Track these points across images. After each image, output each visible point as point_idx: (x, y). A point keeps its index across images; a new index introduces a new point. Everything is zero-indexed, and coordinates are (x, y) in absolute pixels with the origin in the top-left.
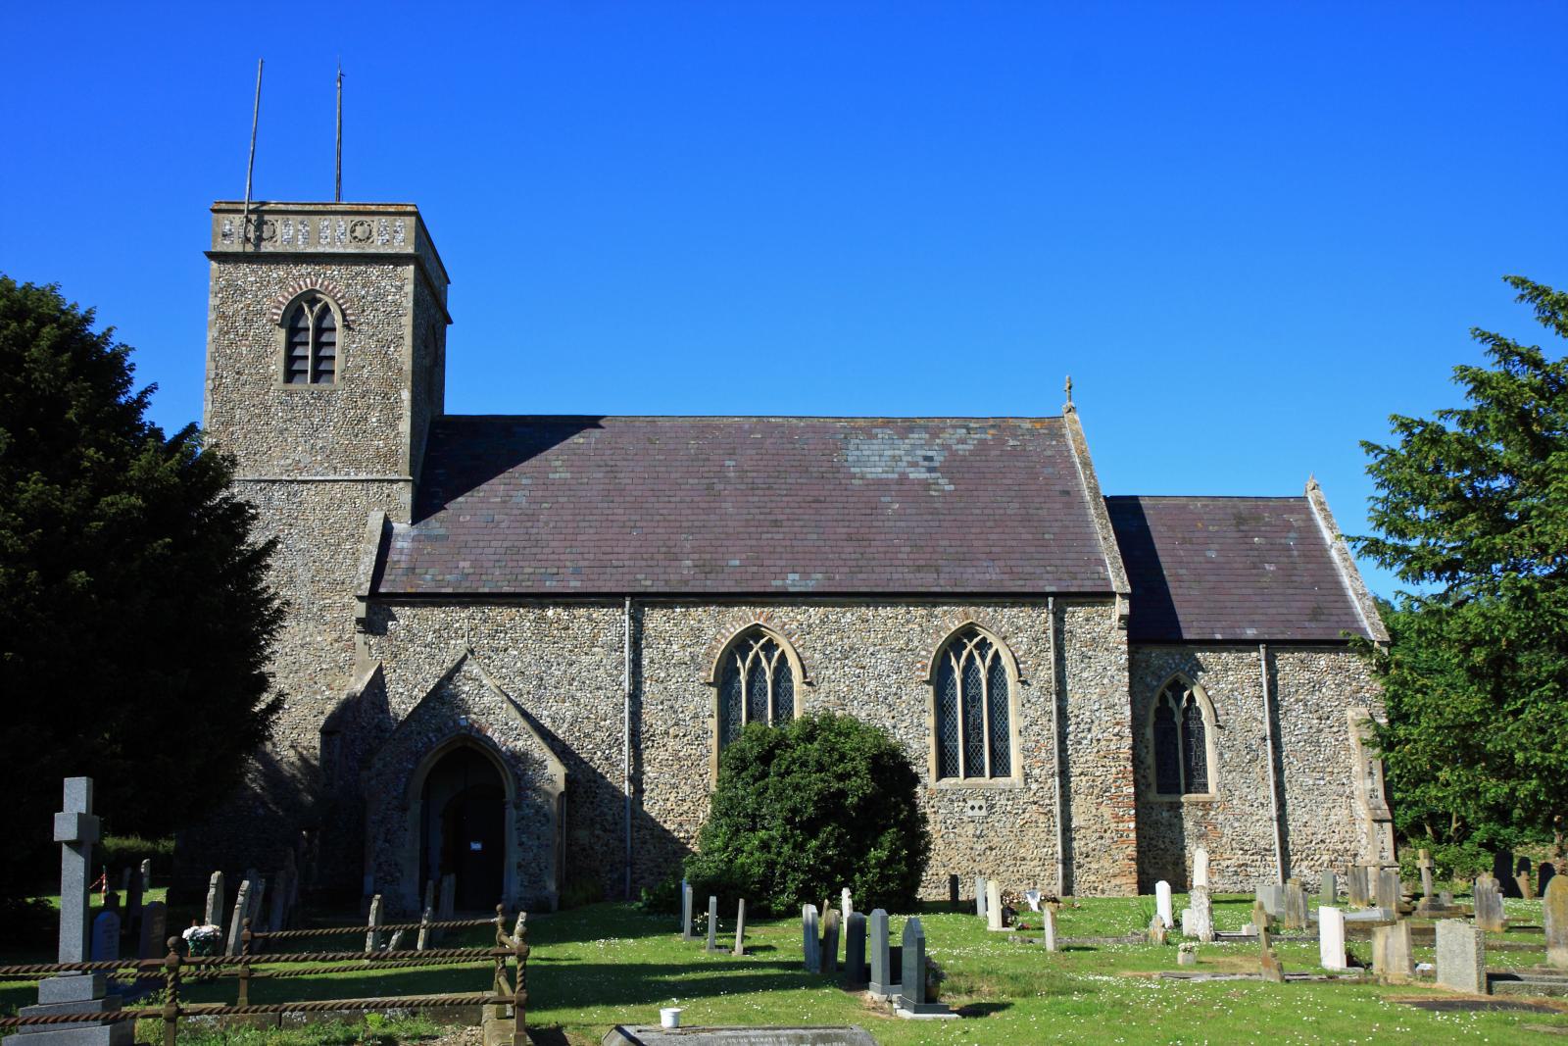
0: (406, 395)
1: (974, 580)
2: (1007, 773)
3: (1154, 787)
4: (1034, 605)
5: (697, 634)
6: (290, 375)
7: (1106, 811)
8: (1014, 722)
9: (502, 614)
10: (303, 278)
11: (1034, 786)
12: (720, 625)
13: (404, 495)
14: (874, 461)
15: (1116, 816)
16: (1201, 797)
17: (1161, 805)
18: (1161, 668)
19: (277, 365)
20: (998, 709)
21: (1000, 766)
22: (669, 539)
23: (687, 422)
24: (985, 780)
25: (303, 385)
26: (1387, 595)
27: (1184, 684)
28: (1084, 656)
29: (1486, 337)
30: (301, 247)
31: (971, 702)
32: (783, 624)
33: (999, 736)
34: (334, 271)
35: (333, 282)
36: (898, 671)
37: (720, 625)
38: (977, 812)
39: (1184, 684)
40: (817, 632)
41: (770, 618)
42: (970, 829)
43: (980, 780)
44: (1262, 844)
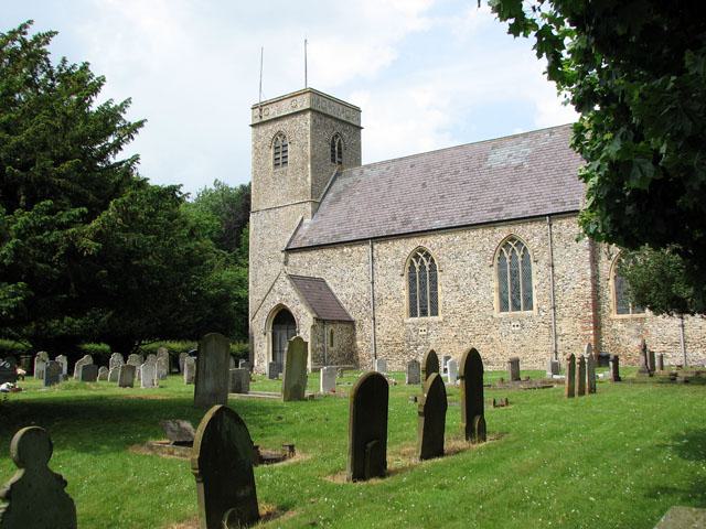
0: (309, 166)
1: (517, 212)
2: (531, 308)
3: (614, 311)
4: (541, 221)
7: (578, 325)
8: (535, 282)
9: (328, 252)
10: (277, 127)
11: (543, 314)
12: (406, 248)
13: (309, 207)
14: (497, 158)
15: (582, 327)
17: (617, 320)
19: (271, 163)
20: (528, 277)
21: (529, 306)
22: (51, 212)
29: (140, 124)
30: (277, 115)
31: (514, 274)
33: (529, 290)
34: (286, 122)
35: (284, 126)
36: (479, 262)
37: (406, 248)
38: (516, 328)
42: (513, 336)
43: (518, 312)
44: (675, 339)
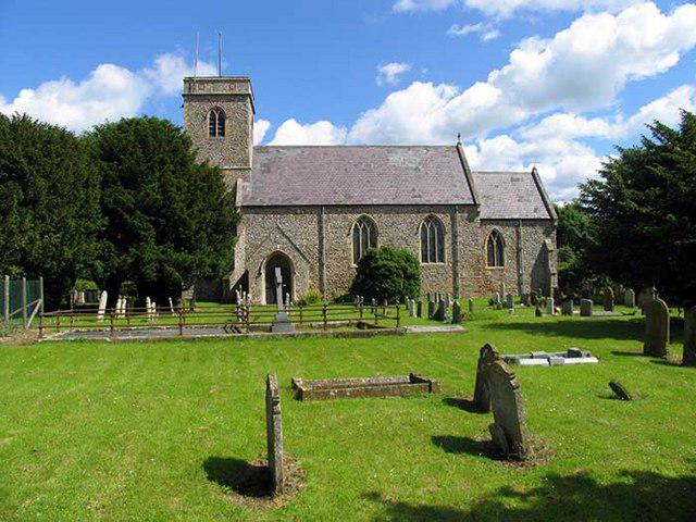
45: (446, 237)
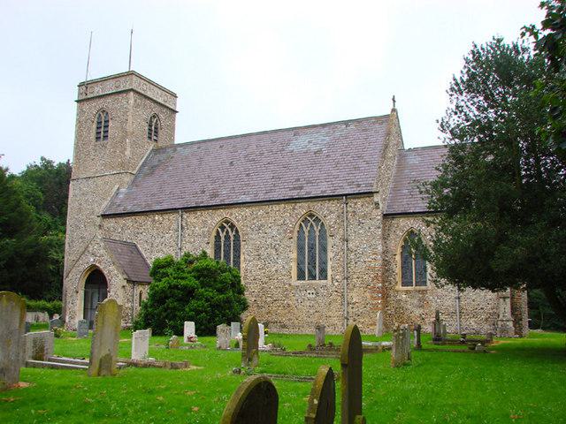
2: (326, 278)
3: (400, 283)
5: (204, 222)
6: (98, 138)
9: (140, 219)
11: (336, 284)
12: (212, 219)
16: (423, 288)
18: (404, 226)
19: (93, 135)
21: (324, 275)
23: (322, 138)
24: (317, 281)
25: (101, 142)
26: (365, 331)
27: (213, 333)
28: (360, 223)
32: (235, 215)
34: (109, 100)
36: (280, 234)
38: (311, 296)
39: (213, 333)
40: (249, 219)
41: (231, 214)
45: (330, 241)
